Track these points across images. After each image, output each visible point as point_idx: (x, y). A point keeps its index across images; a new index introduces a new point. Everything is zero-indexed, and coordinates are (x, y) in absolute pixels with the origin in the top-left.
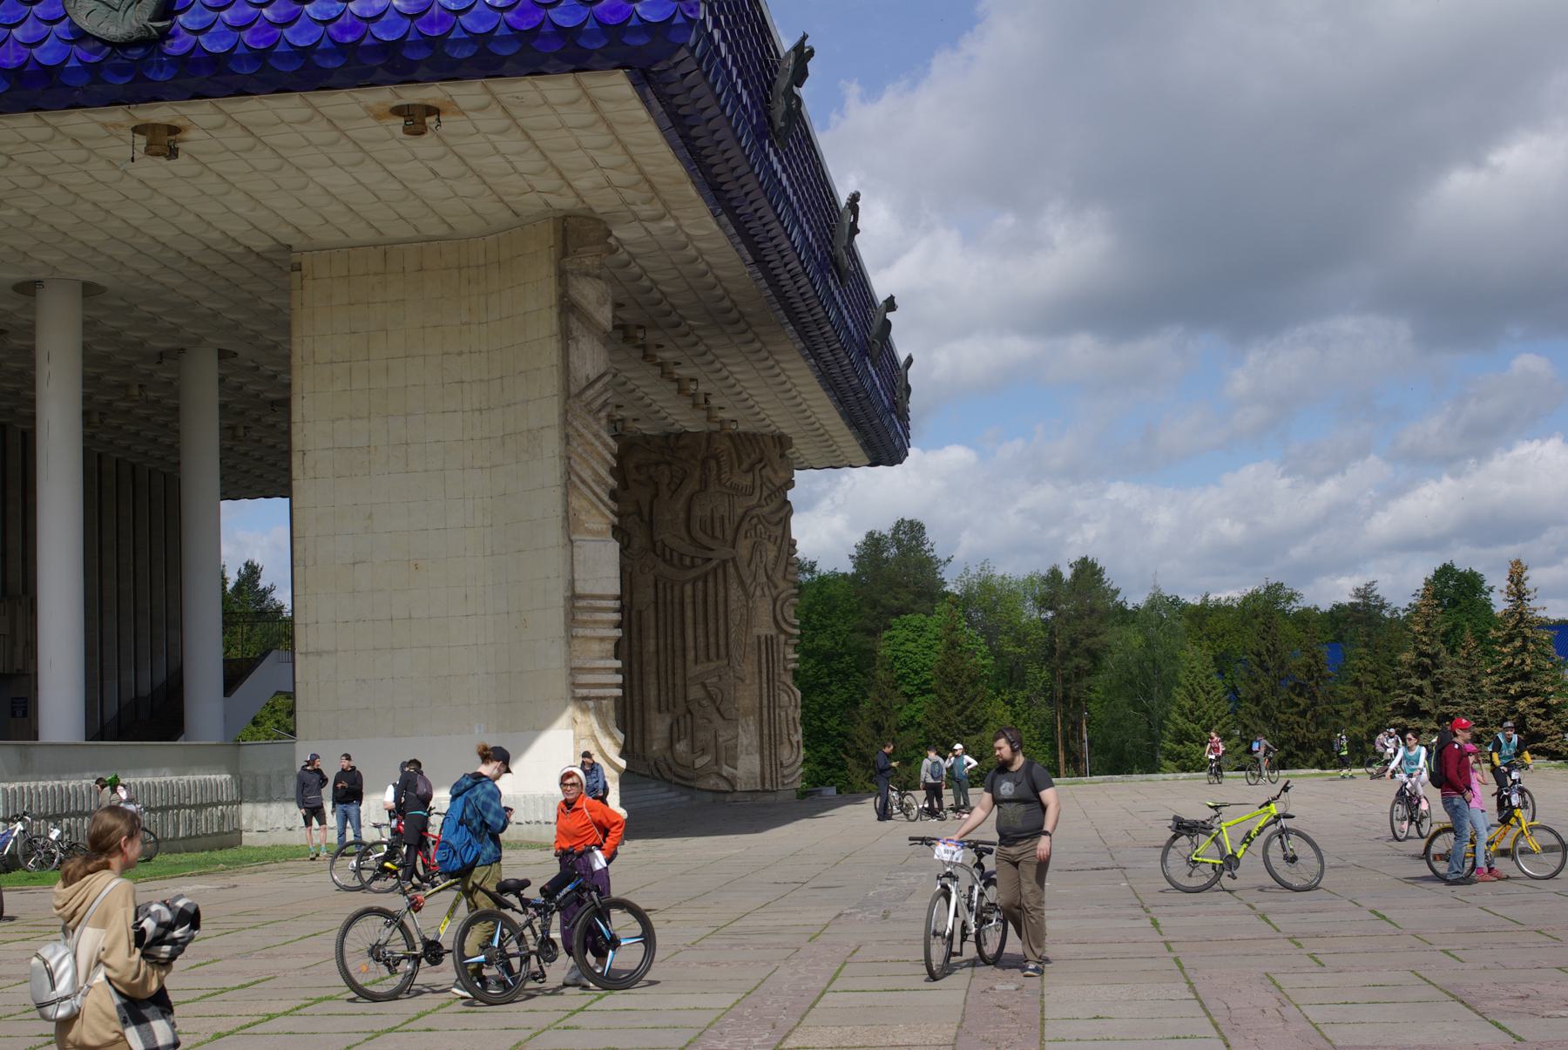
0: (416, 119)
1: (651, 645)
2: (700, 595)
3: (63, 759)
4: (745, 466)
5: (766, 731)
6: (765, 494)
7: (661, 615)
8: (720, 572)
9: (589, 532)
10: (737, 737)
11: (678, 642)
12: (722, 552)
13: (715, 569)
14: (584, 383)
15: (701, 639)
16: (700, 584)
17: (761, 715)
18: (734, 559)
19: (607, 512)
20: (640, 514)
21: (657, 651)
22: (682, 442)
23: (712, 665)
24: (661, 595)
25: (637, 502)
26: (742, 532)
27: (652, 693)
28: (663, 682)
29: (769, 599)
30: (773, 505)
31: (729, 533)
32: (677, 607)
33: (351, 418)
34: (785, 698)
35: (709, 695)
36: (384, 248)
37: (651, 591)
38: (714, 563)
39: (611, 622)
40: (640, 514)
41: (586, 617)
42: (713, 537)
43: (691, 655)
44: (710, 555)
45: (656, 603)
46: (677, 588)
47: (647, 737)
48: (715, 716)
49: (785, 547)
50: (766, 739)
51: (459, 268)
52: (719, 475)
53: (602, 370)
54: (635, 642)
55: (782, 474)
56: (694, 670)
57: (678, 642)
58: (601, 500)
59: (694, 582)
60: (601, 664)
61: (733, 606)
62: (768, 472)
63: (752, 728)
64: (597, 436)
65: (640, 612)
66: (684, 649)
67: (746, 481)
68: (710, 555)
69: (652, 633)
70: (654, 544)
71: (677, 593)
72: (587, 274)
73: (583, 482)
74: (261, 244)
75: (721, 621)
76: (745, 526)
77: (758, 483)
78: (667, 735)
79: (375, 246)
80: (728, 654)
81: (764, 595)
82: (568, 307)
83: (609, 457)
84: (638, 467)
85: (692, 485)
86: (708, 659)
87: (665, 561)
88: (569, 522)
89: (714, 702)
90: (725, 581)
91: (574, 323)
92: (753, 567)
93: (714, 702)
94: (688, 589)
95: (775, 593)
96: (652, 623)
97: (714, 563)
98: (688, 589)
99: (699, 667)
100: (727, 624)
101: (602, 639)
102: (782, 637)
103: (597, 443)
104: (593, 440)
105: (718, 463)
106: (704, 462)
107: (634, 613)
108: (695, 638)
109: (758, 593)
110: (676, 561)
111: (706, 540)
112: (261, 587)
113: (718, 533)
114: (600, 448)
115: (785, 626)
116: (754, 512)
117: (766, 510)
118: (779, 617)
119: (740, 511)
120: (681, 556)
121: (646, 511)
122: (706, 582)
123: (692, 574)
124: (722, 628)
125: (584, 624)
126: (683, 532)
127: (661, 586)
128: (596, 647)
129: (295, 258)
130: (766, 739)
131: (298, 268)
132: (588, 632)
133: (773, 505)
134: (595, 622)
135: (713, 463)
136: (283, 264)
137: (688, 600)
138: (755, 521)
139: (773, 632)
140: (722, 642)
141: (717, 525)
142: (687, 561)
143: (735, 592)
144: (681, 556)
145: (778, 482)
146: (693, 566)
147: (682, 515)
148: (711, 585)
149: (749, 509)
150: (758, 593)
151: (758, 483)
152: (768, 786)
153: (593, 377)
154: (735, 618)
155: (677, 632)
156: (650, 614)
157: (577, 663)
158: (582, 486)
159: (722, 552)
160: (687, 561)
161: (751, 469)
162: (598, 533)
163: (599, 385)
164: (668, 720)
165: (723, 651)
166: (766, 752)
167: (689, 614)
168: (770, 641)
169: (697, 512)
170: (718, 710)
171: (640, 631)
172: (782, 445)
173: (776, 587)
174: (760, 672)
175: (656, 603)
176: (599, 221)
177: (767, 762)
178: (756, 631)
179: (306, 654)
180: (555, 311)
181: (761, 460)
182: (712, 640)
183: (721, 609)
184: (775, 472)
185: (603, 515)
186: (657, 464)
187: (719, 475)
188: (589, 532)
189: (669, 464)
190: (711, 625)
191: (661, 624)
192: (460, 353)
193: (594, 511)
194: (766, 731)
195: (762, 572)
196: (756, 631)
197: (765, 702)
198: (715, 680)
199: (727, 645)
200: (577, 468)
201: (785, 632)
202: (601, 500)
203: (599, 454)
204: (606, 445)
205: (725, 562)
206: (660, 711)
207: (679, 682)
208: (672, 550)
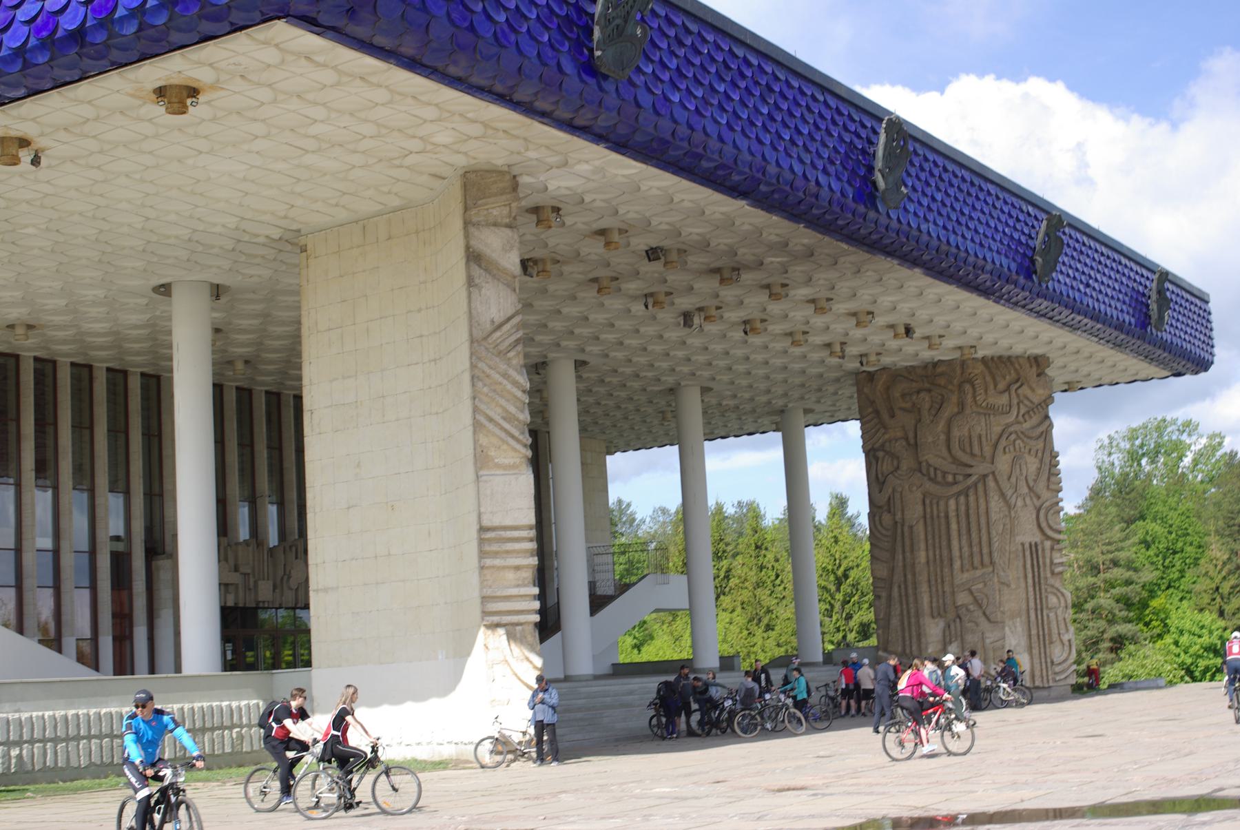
0: (178, 97)
1: (922, 556)
2: (963, 508)
3: (199, 684)
4: (1001, 386)
5: (1034, 632)
6: (1022, 412)
7: (929, 528)
8: (980, 486)
9: (498, 466)
10: (1004, 638)
11: (945, 553)
12: (981, 468)
13: (975, 485)
14: (489, 327)
15: (966, 549)
16: (962, 499)
17: (1029, 617)
18: (993, 473)
19: (519, 447)
20: (907, 439)
21: (928, 562)
22: (939, 370)
23: (978, 573)
24: (928, 510)
25: (903, 427)
26: (1000, 447)
27: (925, 600)
28: (934, 589)
29: (1031, 508)
30: (1035, 420)
31: (987, 450)
32: (943, 521)
33: (344, 378)
34: (1053, 600)
35: (976, 600)
36: (362, 223)
37: (920, 508)
38: (974, 478)
39: (526, 551)
40: (907, 439)
41: (495, 547)
42: (973, 455)
43: (957, 565)
44: (969, 471)
45: (925, 517)
46: (942, 503)
47: (923, 640)
48: (982, 620)
49: (1047, 460)
50: (1034, 638)
51: (417, 232)
52: (974, 397)
53: (510, 312)
54: (908, 554)
55: (1040, 391)
56: (961, 578)
57: (945, 553)
58: (513, 437)
59: (959, 494)
60: (514, 591)
61: (994, 516)
62: (1025, 390)
63: (1019, 629)
64: (505, 375)
65: (911, 527)
66: (951, 560)
67: (1004, 399)
68: (969, 471)
69: (922, 546)
70: (920, 463)
71: (942, 507)
72: (495, 225)
73: (491, 420)
74: (276, 233)
75: (984, 531)
76: (1003, 442)
77: (1015, 401)
78: (940, 637)
79: (357, 222)
80: (992, 563)
81: (1026, 505)
82: (474, 257)
83: (519, 394)
84: (903, 396)
85: (950, 409)
86: (974, 568)
87: (930, 479)
88: (481, 460)
89: (980, 606)
90: (986, 495)
91: (476, 271)
92: (1013, 480)
93: (980, 606)
94: (952, 503)
95: (1038, 504)
96: (922, 536)
97: (974, 478)
98: (952, 503)
99: (966, 575)
100: (989, 533)
101: (517, 568)
102: (1048, 544)
103: (505, 382)
104: (501, 379)
105: (973, 386)
106: (960, 386)
107: (906, 529)
108: (961, 549)
109: (1020, 503)
110: (939, 478)
111: (966, 459)
112: (849, 514)
113: (976, 450)
114: (509, 386)
115: (1050, 533)
116: (1012, 429)
117: (1027, 425)
118: (1044, 525)
119: (997, 430)
120: (945, 473)
121: (911, 435)
122: (967, 496)
123: (956, 489)
124: (985, 538)
125: (496, 554)
126: (945, 452)
127: (927, 502)
128: (510, 575)
129: (303, 240)
130: (1034, 638)
131: (304, 249)
132: (498, 562)
133: (1035, 420)
134: (507, 552)
135: (967, 387)
136: (294, 245)
137: (952, 514)
138: (1013, 437)
139: (1037, 538)
140: (985, 551)
141: (976, 443)
142: (950, 478)
143: (995, 504)
144: (945, 473)
145: (1036, 400)
146: (955, 483)
147: (943, 437)
148: (972, 498)
149: (1008, 426)
150: (1020, 503)
151: (1015, 401)
152: (1037, 683)
153: (498, 320)
154: (996, 530)
155: (944, 543)
156: (920, 529)
157: (489, 592)
158: (491, 426)
159: (981, 468)
160: (950, 478)
161: (1008, 389)
162: (513, 467)
163: (507, 327)
164: (942, 624)
165: (986, 559)
166: (1036, 651)
167: (954, 526)
168: (1034, 548)
169: (956, 433)
170: (984, 613)
171: (912, 545)
172: (1038, 365)
173: (1039, 498)
174: (1026, 577)
175: (925, 517)
176: (501, 173)
177: (1036, 661)
178: (1019, 539)
179: (317, 591)
180: (464, 261)
181: (1017, 381)
182: (975, 549)
183: (983, 521)
184: (1033, 390)
185: (515, 450)
186: (918, 392)
187: (974, 397)
188: (498, 466)
189: (929, 391)
190: (974, 535)
191: (930, 537)
192: (420, 310)
193: (505, 447)
194: (1034, 632)
195: (1022, 483)
196: (1019, 539)
197: (1032, 604)
198: (981, 586)
199: (991, 553)
200: (482, 407)
201: (1048, 538)
202: (513, 437)
203: (509, 392)
204: (515, 383)
205: (985, 476)
206: (933, 617)
207: (947, 589)
208: (935, 469)
